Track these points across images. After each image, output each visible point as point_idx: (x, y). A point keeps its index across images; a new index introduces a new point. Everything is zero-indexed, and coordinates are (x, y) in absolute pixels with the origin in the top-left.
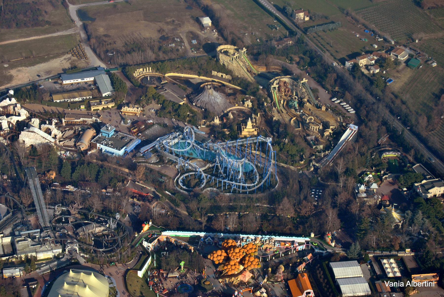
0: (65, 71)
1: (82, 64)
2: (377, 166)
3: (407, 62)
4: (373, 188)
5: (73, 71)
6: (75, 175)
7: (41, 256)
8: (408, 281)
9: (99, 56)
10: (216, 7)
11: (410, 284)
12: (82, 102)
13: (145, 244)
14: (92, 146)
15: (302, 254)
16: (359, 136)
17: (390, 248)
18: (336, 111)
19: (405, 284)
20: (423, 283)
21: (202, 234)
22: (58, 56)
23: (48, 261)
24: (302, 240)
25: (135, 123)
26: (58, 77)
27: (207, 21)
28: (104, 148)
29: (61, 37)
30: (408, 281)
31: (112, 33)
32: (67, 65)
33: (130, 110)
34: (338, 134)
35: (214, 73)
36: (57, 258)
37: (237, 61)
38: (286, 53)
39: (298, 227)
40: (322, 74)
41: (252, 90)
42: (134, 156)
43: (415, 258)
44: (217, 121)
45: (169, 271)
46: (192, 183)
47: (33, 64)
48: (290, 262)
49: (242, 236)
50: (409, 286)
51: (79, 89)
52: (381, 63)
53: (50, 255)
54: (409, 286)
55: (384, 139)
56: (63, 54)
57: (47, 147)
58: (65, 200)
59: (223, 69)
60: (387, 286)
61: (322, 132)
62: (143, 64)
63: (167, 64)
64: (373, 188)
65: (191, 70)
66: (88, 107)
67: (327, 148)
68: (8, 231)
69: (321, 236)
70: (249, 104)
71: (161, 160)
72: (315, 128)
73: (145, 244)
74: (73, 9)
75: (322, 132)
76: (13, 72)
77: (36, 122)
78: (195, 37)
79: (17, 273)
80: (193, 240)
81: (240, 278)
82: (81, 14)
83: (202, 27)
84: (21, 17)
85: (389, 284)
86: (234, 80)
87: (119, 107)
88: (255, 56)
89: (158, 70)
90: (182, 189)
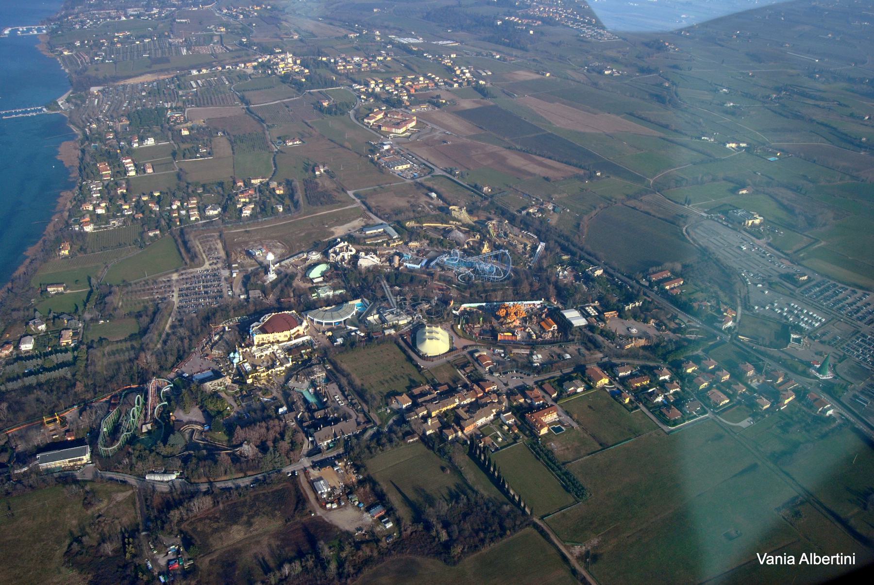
0: (364, 227)
1: (371, 222)
2: (562, 263)
3: (553, 210)
4: (564, 274)
5: (368, 226)
6: (398, 281)
7: (401, 323)
8: (804, 554)
9: (380, 218)
10: (435, 187)
11: (806, 560)
12: (383, 242)
13: (454, 312)
14: (400, 265)
15: (541, 309)
16: (546, 249)
17: (587, 301)
18: (529, 237)
19: (797, 560)
20: (832, 557)
21: (484, 304)
22: (354, 219)
23: (406, 325)
24: (539, 302)
25: (418, 252)
26: (362, 230)
27: (434, 195)
28: (408, 265)
29: (351, 209)
30: (804, 554)
31: (381, 204)
32: (363, 224)
33: (413, 244)
34: (534, 248)
35: (451, 222)
36: (409, 323)
37: (461, 214)
38: (486, 209)
39: (533, 296)
40: (512, 220)
41: (479, 228)
42: (427, 268)
43: (601, 305)
44: (466, 246)
45: (474, 324)
46: (467, 279)
47: (343, 224)
48: (538, 313)
49: (506, 303)
50: (804, 563)
51: (376, 236)
52: (541, 210)
53: (405, 322)
54: (804, 563)
55: (558, 250)
56: (358, 217)
57: (375, 266)
58: (400, 293)
59: (455, 219)
60: (762, 563)
61: (525, 248)
62: (410, 220)
63: (423, 219)
64: (564, 274)
65: (437, 221)
66: (388, 244)
67: (530, 256)
68: (375, 312)
69: (548, 299)
70: (478, 236)
71: (443, 269)
72: (520, 247)
73: (454, 312)
74: (350, 193)
75: (525, 248)
76: (332, 229)
77: (362, 254)
78: (430, 204)
79: (393, 332)
80: (480, 308)
81: (514, 323)
82: (357, 195)
83: (432, 198)
84: (322, 199)
85: (766, 559)
86: (463, 225)
87: (406, 244)
88: (470, 212)
89: (418, 222)
90: (462, 283)
